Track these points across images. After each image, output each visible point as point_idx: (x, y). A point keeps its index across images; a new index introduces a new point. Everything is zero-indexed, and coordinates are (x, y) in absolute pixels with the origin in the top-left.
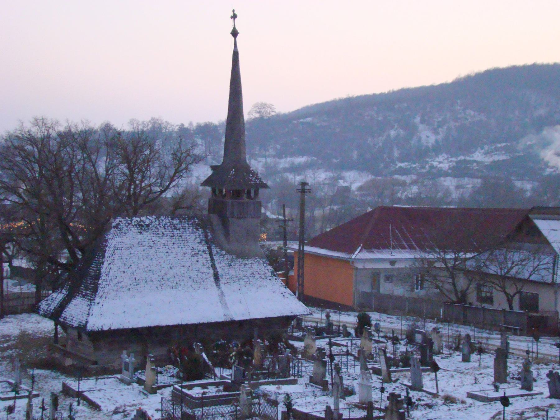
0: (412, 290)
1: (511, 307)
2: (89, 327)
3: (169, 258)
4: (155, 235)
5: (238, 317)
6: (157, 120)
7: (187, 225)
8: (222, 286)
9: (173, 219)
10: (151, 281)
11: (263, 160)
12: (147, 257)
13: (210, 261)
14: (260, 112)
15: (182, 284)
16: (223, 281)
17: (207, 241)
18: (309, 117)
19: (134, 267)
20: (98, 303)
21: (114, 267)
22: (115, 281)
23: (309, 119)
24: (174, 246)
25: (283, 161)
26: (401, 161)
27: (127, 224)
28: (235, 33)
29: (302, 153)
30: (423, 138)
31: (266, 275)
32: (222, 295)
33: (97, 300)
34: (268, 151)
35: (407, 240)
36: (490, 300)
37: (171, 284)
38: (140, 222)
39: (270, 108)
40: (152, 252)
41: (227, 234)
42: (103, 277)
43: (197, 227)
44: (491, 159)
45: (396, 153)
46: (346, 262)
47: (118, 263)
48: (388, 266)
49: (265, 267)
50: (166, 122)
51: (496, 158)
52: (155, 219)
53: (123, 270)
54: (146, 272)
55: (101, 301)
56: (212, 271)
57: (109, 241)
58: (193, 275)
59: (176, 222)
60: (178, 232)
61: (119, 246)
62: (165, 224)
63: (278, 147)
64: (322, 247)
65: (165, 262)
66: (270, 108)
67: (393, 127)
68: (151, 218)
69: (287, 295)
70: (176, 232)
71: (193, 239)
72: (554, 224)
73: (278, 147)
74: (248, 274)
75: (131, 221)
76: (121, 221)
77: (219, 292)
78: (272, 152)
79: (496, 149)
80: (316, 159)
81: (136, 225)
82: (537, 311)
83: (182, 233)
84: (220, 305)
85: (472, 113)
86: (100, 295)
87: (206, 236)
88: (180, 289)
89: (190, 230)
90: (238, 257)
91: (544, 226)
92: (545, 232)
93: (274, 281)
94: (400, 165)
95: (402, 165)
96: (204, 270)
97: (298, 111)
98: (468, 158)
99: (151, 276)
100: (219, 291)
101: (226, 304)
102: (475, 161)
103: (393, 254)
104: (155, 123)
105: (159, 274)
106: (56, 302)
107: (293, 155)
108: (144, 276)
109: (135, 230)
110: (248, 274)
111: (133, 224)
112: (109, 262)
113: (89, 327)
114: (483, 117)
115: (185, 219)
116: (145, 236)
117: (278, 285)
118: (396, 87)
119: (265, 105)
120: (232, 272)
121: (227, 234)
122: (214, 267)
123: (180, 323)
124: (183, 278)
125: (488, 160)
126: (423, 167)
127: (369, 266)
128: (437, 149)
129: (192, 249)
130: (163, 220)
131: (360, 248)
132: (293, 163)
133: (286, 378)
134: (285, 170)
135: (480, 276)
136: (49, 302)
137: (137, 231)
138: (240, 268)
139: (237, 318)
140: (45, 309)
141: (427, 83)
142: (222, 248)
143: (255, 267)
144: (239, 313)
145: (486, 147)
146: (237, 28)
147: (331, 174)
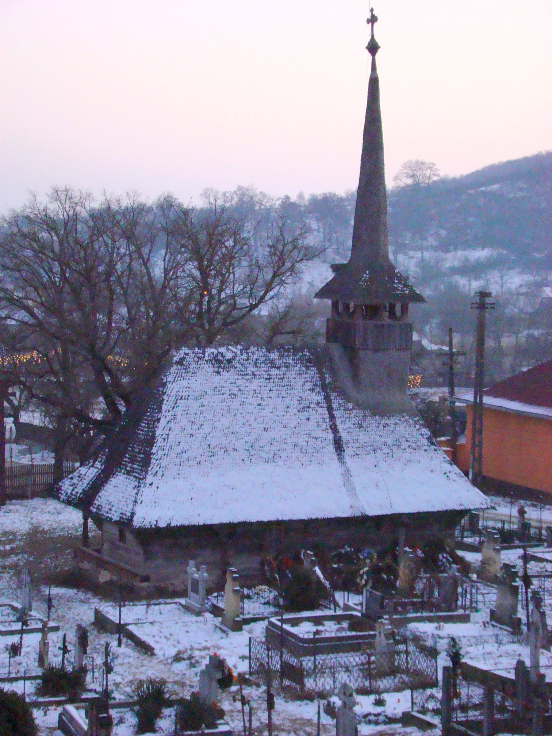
2: (137, 522)
3: (264, 413)
4: (240, 377)
6: (247, 190)
7: (291, 361)
8: (348, 459)
9: (269, 351)
10: (235, 450)
11: (418, 254)
12: (229, 411)
14: (413, 176)
16: (348, 452)
17: (324, 387)
18: (492, 184)
19: (207, 428)
20: (151, 484)
22: (179, 449)
24: (271, 395)
25: (450, 256)
27: (196, 359)
28: (373, 48)
31: (418, 443)
32: (347, 474)
33: (150, 478)
34: (426, 239)
37: (266, 456)
38: (217, 355)
39: (431, 168)
40: (235, 403)
41: (355, 377)
42: (159, 442)
43: (308, 363)
47: (182, 420)
49: (418, 430)
50: (261, 193)
52: (241, 350)
54: (226, 436)
56: (331, 436)
57: (169, 385)
58: (301, 441)
59: (274, 355)
62: (257, 359)
66: (431, 168)
68: (234, 350)
69: (453, 476)
70: (274, 372)
71: (301, 383)
73: (443, 233)
74: (390, 441)
75: (204, 353)
76: (187, 354)
77: (341, 470)
78: (431, 241)
81: (211, 361)
83: (284, 374)
84: (344, 489)
87: (322, 379)
89: (297, 368)
90: (374, 415)
93: (432, 453)
96: (318, 433)
97: (477, 173)
99: (233, 441)
101: (354, 489)
104: (243, 194)
105: (247, 438)
106: (86, 482)
107: (467, 246)
108: (224, 441)
109: (209, 369)
110: (390, 441)
111: (206, 358)
112: (168, 419)
113: (137, 522)
115: (288, 351)
116: (225, 378)
117: (439, 460)
119: (423, 163)
120: (363, 437)
122: (334, 428)
123: (280, 519)
124: (285, 446)
130: (253, 353)
132: (467, 260)
133: (453, 611)
134: (454, 271)
137: (212, 369)
138: (375, 432)
139: (372, 512)
142: (348, 399)
144: (375, 505)
146: (377, 39)
147: (531, 278)
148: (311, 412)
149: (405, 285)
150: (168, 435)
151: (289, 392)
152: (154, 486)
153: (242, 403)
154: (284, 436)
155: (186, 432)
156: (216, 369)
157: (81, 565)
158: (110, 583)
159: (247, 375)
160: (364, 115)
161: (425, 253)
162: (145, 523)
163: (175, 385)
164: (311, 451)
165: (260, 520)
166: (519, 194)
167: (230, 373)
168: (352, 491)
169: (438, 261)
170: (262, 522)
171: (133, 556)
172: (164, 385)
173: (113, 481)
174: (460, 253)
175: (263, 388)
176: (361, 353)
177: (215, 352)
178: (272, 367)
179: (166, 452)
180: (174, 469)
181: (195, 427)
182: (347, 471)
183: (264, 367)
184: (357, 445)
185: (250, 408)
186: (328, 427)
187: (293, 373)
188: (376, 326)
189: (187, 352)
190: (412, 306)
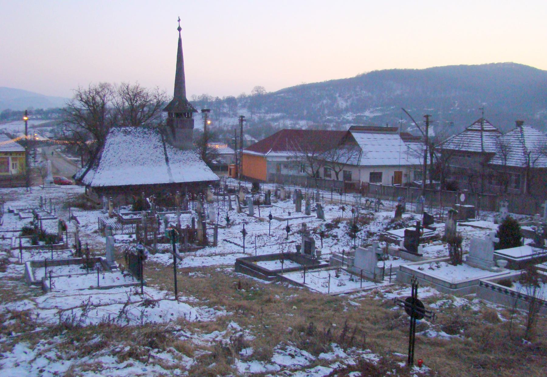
1: (337, 178)
2: (92, 185)
11: (259, 115)
16: (170, 162)
17: (163, 141)
21: (109, 154)
23: (282, 95)
26: (329, 116)
28: (179, 29)
29: (278, 111)
30: (340, 104)
32: (169, 169)
33: (98, 171)
36: (330, 176)
40: (131, 146)
41: (174, 137)
42: (103, 159)
43: (158, 133)
44: (373, 115)
45: (326, 112)
46: (262, 157)
47: (111, 151)
48: (285, 160)
51: (376, 115)
55: (100, 171)
56: (164, 157)
58: (154, 158)
59: (146, 130)
67: (325, 99)
69: (207, 170)
70: (145, 135)
71: (155, 139)
72: (362, 135)
74: (185, 159)
78: (263, 111)
79: (376, 110)
82: (351, 180)
85: (365, 92)
87: (162, 137)
90: (180, 150)
91: (355, 135)
92: (357, 140)
93: (200, 162)
94: (328, 117)
95: (329, 117)
96: (160, 156)
98: (362, 115)
102: (365, 116)
109: (122, 134)
110: (185, 159)
113: (92, 185)
114: (370, 94)
117: (203, 165)
118: (328, 79)
120: (176, 157)
121: (174, 137)
122: (166, 154)
125: (372, 115)
126: (339, 119)
127: (275, 160)
128: (347, 110)
129: (154, 145)
132: (273, 117)
134: (269, 120)
135: (323, 162)
138: (180, 155)
139: (176, 182)
141: (343, 78)
142: (171, 145)
143: (190, 154)
144: (178, 179)
145: (371, 109)
153: (134, 146)
163: (110, 140)
171: (95, 197)
173: (89, 172)
174: (271, 114)
180: (107, 168)
182: (170, 168)
183: (142, 134)
185: (136, 147)
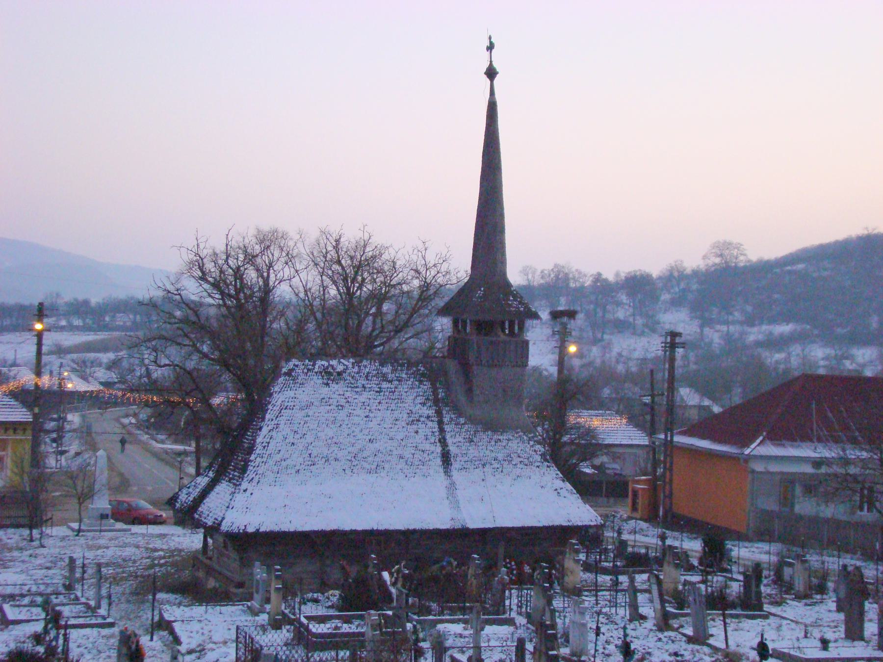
0: (854, 513)
3: (371, 425)
4: (349, 389)
5: (474, 524)
6: (563, 267)
7: (404, 376)
8: (455, 473)
9: (382, 365)
10: (336, 459)
11: (724, 328)
12: (334, 422)
13: (437, 434)
14: (721, 255)
15: (387, 466)
16: (456, 465)
17: (436, 401)
18: (798, 263)
19: (309, 438)
20: (245, 491)
21: (278, 436)
22: (278, 457)
23: (800, 266)
24: (379, 407)
25: (755, 330)
27: (306, 371)
31: (531, 459)
32: (452, 487)
33: (245, 485)
34: (731, 314)
35: (846, 428)
37: (368, 467)
38: (327, 368)
39: (738, 249)
40: (342, 414)
41: (469, 391)
42: (259, 450)
43: (421, 378)
47: (285, 429)
48: (808, 469)
49: (532, 446)
50: (577, 270)
52: (353, 364)
53: (292, 441)
54: (329, 446)
56: (439, 449)
57: (275, 395)
58: (407, 454)
59: (387, 369)
60: (389, 385)
61: (289, 404)
62: (368, 373)
63: (749, 308)
64: (702, 437)
65: (361, 431)
66: (738, 249)
68: (346, 363)
69: (563, 492)
70: (385, 385)
71: (412, 397)
73: (749, 308)
74: (500, 456)
75: (314, 365)
76: (297, 366)
77: (447, 482)
78: (737, 315)
80: (808, 327)
81: (321, 373)
83: (396, 388)
84: (447, 502)
86: (250, 477)
88: (382, 474)
89: (410, 383)
96: (427, 446)
97: (787, 256)
99: (336, 452)
100: (449, 481)
101: (457, 502)
103: (818, 450)
104: (559, 272)
105: (350, 449)
106: (198, 490)
107: (773, 321)
108: (326, 451)
110: (500, 456)
111: (316, 370)
112: (270, 428)
115: (402, 365)
116: (333, 390)
117: (551, 476)
119: (730, 244)
120: (473, 452)
122: (443, 442)
123: (375, 528)
124: (389, 458)
127: (775, 468)
130: (365, 367)
131: (761, 438)
132: (771, 333)
133: (498, 615)
134: (758, 344)
136: (191, 490)
137: (320, 381)
138: (486, 446)
139: (472, 525)
140: (184, 500)
143: (514, 445)
144: (476, 517)
146: (495, 65)
147: (833, 352)
148: (420, 425)
149: (520, 303)
150: (269, 443)
151: (399, 405)
152: (248, 492)
153: (349, 415)
154: (389, 448)
155: (287, 440)
156: (325, 381)
157: (197, 574)
158: (215, 589)
159: (357, 387)
160: (483, 138)
161: (731, 327)
162: (233, 527)
163: (281, 395)
164: (417, 463)
165: (354, 528)
166: (825, 273)
167: (339, 385)
168: (455, 504)
169: (743, 334)
170: (355, 530)
172: (271, 394)
173: (218, 488)
174: (764, 327)
175: (372, 401)
176: (475, 367)
177: (326, 364)
178: (383, 381)
179: (265, 460)
181: (298, 436)
182: (453, 484)
183: (375, 381)
184: (464, 459)
186: (437, 441)
187: (405, 386)
188: (491, 343)
189: (296, 363)
190: (529, 323)
